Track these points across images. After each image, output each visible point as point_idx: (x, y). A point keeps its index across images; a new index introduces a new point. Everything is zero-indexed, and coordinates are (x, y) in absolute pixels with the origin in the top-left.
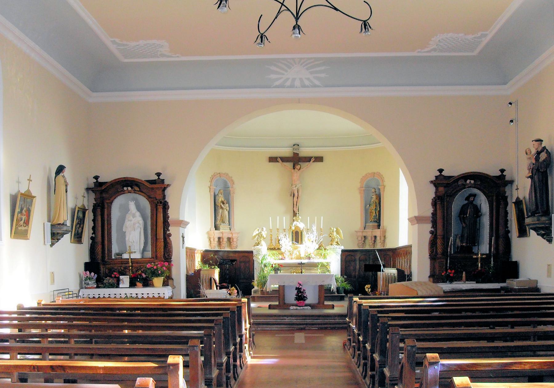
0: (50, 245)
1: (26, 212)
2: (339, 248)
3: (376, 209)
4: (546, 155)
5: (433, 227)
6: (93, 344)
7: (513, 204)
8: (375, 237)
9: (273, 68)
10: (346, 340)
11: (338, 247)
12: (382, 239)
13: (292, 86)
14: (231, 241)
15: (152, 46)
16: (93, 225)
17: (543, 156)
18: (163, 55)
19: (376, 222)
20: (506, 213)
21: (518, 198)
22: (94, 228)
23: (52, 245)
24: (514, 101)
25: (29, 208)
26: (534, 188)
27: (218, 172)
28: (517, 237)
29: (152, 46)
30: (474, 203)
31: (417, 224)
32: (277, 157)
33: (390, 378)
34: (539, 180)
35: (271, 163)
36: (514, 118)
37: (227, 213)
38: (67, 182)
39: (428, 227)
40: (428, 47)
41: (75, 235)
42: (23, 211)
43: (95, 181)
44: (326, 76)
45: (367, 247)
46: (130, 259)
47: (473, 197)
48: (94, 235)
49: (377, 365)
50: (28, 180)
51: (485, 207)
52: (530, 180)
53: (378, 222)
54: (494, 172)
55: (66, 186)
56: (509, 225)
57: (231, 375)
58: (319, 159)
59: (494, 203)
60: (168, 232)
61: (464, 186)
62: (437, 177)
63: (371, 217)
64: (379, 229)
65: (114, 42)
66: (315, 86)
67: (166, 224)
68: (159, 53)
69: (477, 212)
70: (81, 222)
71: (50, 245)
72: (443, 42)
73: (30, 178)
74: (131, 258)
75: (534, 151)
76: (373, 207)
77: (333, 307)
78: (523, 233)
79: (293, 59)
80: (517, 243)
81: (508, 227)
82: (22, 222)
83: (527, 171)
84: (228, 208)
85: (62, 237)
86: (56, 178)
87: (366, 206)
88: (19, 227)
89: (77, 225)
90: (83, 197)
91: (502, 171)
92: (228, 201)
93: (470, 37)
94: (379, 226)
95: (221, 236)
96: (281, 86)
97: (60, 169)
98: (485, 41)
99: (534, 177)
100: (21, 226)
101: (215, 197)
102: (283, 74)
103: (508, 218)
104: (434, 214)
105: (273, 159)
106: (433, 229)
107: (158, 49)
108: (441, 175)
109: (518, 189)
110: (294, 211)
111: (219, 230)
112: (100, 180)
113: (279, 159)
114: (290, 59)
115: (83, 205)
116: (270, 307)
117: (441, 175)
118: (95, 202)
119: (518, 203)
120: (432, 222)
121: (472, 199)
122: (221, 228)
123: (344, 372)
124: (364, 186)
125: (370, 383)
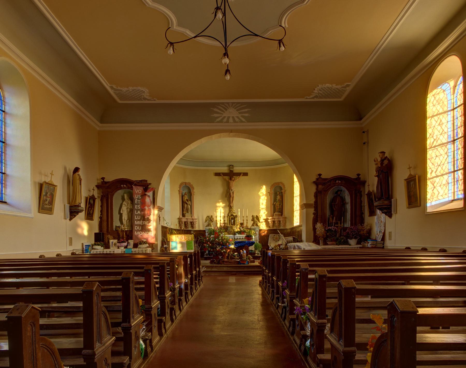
1: (50, 196)
3: (280, 204)
4: (387, 161)
7: (366, 195)
9: (216, 110)
13: (228, 122)
15: (138, 92)
16: (101, 209)
17: (386, 162)
18: (145, 99)
20: (361, 202)
21: (369, 191)
26: (380, 182)
27: (184, 182)
28: (368, 216)
29: (138, 92)
30: (341, 195)
31: (305, 209)
33: (290, 296)
37: (189, 207)
39: (312, 210)
40: (312, 95)
42: (48, 195)
43: (102, 181)
44: (249, 115)
47: (340, 192)
48: (101, 216)
51: (348, 199)
53: (281, 212)
54: (353, 176)
56: (363, 209)
58: (246, 174)
62: (317, 179)
64: (282, 216)
65: (112, 88)
66: (242, 122)
68: (143, 97)
69: (343, 200)
72: (322, 91)
75: (379, 159)
78: (372, 213)
79: (228, 103)
81: (362, 211)
82: (47, 202)
83: (375, 173)
84: (190, 204)
85: (77, 214)
88: (45, 205)
89: (89, 208)
91: (358, 175)
92: (190, 199)
93: (339, 87)
94: (282, 215)
95: (186, 220)
96: (221, 121)
98: (349, 89)
99: (380, 176)
101: (182, 196)
102: (223, 114)
104: (316, 202)
105: (217, 174)
106: (315, 212)
107: (142, 94)
109: (369, 185)
111: (185, 217)
112: (105, 180)
114: (226, 103)
117: (320, 178)
118: (102, 194)
119: (369, 194)
120: (315, 207)
121: (340, 193)
122: (186, 216)
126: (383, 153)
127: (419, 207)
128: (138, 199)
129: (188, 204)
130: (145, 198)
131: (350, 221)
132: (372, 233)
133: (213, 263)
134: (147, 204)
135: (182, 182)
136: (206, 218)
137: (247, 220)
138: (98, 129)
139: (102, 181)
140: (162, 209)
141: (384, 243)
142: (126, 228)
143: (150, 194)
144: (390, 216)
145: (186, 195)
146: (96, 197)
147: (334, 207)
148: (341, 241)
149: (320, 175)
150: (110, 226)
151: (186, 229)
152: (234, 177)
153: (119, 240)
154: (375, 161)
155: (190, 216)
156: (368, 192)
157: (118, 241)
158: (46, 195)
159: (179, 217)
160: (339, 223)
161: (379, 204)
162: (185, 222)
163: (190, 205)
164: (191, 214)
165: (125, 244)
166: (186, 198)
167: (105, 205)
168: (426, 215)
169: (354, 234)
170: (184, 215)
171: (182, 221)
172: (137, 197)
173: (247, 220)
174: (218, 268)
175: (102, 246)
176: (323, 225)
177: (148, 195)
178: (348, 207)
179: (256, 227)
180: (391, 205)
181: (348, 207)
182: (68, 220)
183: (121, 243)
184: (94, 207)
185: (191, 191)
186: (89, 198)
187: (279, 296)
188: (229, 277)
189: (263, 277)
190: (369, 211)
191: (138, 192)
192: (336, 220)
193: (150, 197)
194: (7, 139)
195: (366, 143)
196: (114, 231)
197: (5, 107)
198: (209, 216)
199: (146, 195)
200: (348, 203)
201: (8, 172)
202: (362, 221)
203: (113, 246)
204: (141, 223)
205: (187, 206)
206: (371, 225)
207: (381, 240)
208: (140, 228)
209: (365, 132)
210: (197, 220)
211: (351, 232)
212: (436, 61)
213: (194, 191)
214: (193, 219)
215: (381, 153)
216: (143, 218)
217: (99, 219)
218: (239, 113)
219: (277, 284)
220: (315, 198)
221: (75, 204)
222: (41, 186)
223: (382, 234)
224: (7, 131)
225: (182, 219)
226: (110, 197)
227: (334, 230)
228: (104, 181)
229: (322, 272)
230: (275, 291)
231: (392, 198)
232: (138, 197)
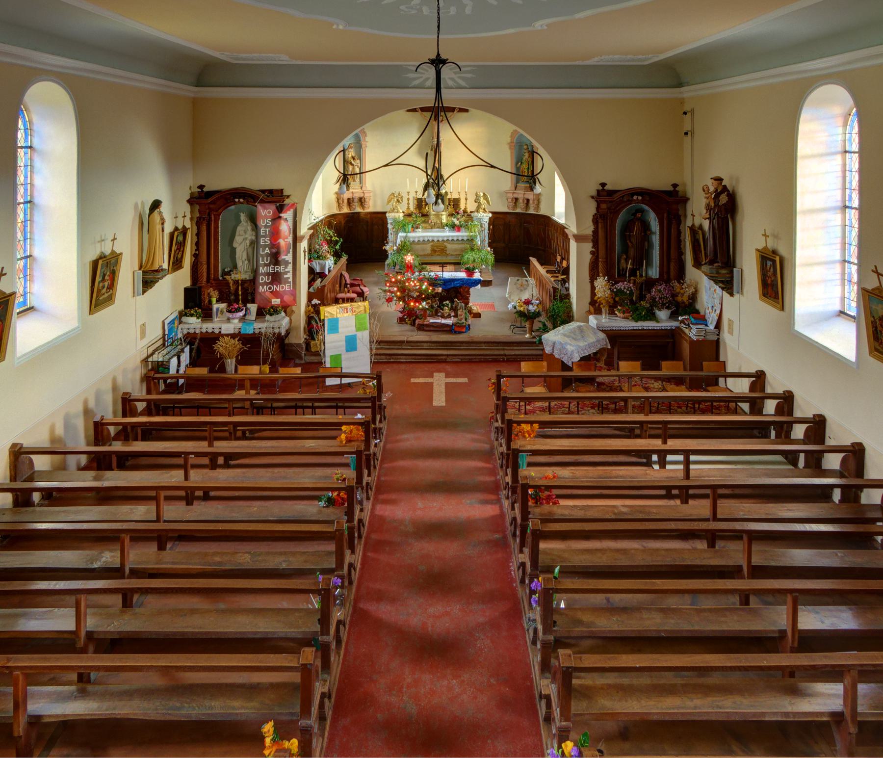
2: (487, 216)
3: (528, 168)
5: (594, 246)
8: (528, 200)
11: (485, 215)
12: (536, 202)
14: (363, 201)
16: (197, 240)
20: (679, 233)
22: (197, 244)
23: (144, 292)
24: (689, 110)
34: (718, 227)
41: (173, 263)
45: (518, 210)
48: (197, 252)
51: (655, 225)
55: (163, 224)
56: (682, 246)
59: (665, 222)
61: (630, 202)
69: (646, 227)
70: (181, 246)
75: (712, 189)
81: (681, 249)
84: (359, 165)
87: (517, 163)
91: (675, 186)
95: (350, 196)
97: (156, 205)
102: (424, 74)
103: (682, 238)
104: (595, 232)
106: (593, 250)
108: (603, 190)
117: (603, 190)
120: (593, 241)
124: (515, 141)
126: (719, 180)
128: (266, 226)
130: (280, 224)
131: (660, 267)
132: (699, 299)
133: (403, 323)
134: (282, 235)
136: (389, 197)
137: (466, 199)
138: (192, 95)
141: (719, 332)
142: (242, 273)
143: (288, 215)
144: (732, 295)
147: (628, 241)
148: (641, 313)
150: (212, 272)
153: (230, 305)
154: (704, 191)
157: (229, 306)
162: (349, 199)
164: (361, 184)
165: (241, 314)
166: (351, 153)
167: (204, 234)
169: (667, 303)
172: (263, 223)
173: (466, 199)
174: (412, 344)
175: (198, 318)
176: (609, 282)
177: (285, 217)
178: (656, 240)
179: (482, 214)
180: (732, 277)
181: (656, 240)
183: (234, 312)
184: (184, 246)
185: (360, 140)
190: (694, 258)
191: (266, 214)
192: (633, 264)
193: (287, 221)
194: (36, 194)
196: (221, 280)
197: (33, 138)
199: (280, 217)
200: (655, 233)
201: (36, 253)
202: (681, 274)
203: (219, 315)
204: (271, 269)
206: (697, 283)
208: (268, 279)
210: (371, 194)
211: (660, 298)
213: (366, 140)
216: (273, 261)
217: (193, 259)
218: (454, 72)
220: (594, 225)
221: (153, 269)
224: (35, 180)
226: (213, 219)
227: (628, 292)
228: (202, 191)
231: (734, 266)
232: (267, 223)
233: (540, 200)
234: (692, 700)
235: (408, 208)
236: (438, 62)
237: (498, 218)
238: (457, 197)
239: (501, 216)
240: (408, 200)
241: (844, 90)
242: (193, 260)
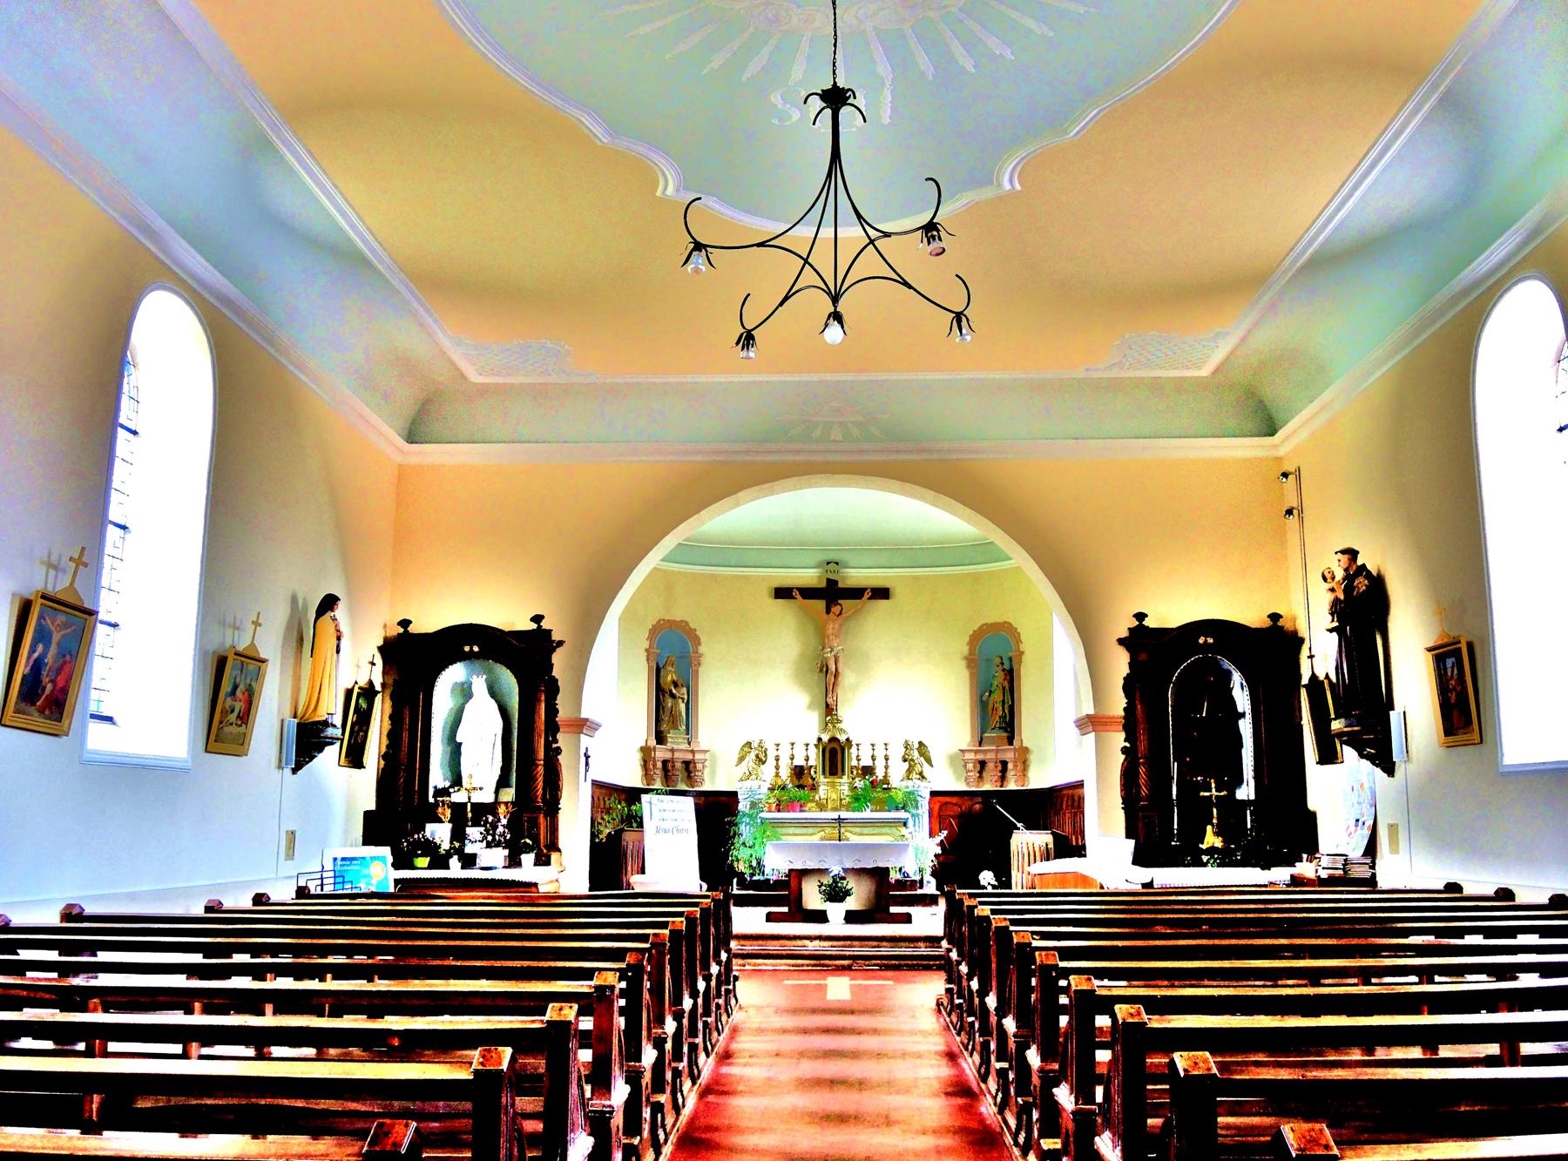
0: (292, 769)
3: (1003, 701)
6: (558, 745)
10: (943, 992)
17: (1361, 584)
19: (1005, 730)
21: (1314, 677)
25: (250, 685)
31: (1093, 734)
32: (793, 588)
35: (777, 600)
36: (1295, 505)
37: (682, 707)
38: (341, 630)
43: (401, 630)
46: (469, 805)
49: (1012, 1045)
50: (260, 625)
52: (1335, 636)
55: (339, 638)
57: (699, 1040)
58: (882, 593)
60: (554, 746)
63: (995, 719)
67: (553, 728)
70: (364, 719)
71: (292, 769)
73: (255, 629)
74: (472, 801)
75: (1340, 574)
76: (997, 696)
77: (907, 919)
80: (1316, 774)
82: (233, 717)
84: (686, 697)
86: (318, 622)
90: (370, 666)
94: (1010, 741)
95: (668, 756)
100: (231, 724)
101: (658, 670)
105: (782, 593)
106: (1127, 745)
110: (827, 705)
113: (796, 593)
115: (371, 683)
116: (771, 918)
119: (1315, 684)
122: (669, 740)
123: (939, 1066)
125: (998, 1091)
127: (1478, 744)
129: (679, 697)
135: (660, 621)
137: (887, 759)
138: (399, 459)
139: (401, 630)
140: (596, 726)
141: (1374, 862)
145: (673, 664)
146: (378, 687)
149: (1140, 616)
151: (668, 786)
152: (841, 605)
154: (1325, 579)
155: (684, 739)
156: (1310, 679)
158: (233, 693)
159: (644, 745)
160: (1213, 785)
161: (1346, 727)
162: (665, 762)
163: (683, 699)
168: (1503, 774)
170: (660, 738)
171: (654, 758)
173: (887, 759)
181: (1246, 727)
182: (288, 771)
186: (356, 691)
187: (1005, 1065)
188: (825, 979)
189: (952, 986)
195: (1295, 512)
198: (750, 743)
205: (677, 704)
207: (1365, 854)
209: (1291, 473)
210: (707, 756)
212: (1489, 289)
213: (700, 652)
214: (693, 752)
215: (1343, 552)
219: (1000, 1025)
222: (221, 663)
223: (1366, 833)
225: (655, 751)
228: (406, 631)
229: (1132, 1015)
230: (993, 1046)
233: (1028, 763)
234: (1311, 1072)
235: (777, 775)
236: (835, 98)
237: (947, 803)
238: (870, 763)
239: (954, 800)
240: (777, 760)
241: (1545, 286)
242: (382, 766)
